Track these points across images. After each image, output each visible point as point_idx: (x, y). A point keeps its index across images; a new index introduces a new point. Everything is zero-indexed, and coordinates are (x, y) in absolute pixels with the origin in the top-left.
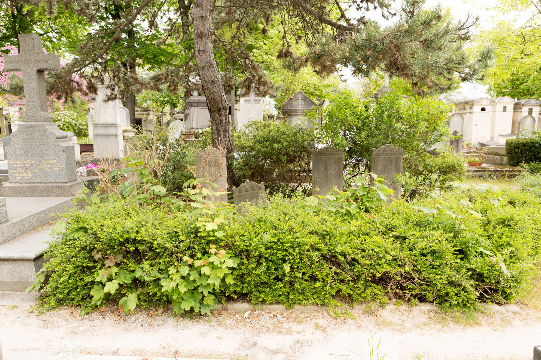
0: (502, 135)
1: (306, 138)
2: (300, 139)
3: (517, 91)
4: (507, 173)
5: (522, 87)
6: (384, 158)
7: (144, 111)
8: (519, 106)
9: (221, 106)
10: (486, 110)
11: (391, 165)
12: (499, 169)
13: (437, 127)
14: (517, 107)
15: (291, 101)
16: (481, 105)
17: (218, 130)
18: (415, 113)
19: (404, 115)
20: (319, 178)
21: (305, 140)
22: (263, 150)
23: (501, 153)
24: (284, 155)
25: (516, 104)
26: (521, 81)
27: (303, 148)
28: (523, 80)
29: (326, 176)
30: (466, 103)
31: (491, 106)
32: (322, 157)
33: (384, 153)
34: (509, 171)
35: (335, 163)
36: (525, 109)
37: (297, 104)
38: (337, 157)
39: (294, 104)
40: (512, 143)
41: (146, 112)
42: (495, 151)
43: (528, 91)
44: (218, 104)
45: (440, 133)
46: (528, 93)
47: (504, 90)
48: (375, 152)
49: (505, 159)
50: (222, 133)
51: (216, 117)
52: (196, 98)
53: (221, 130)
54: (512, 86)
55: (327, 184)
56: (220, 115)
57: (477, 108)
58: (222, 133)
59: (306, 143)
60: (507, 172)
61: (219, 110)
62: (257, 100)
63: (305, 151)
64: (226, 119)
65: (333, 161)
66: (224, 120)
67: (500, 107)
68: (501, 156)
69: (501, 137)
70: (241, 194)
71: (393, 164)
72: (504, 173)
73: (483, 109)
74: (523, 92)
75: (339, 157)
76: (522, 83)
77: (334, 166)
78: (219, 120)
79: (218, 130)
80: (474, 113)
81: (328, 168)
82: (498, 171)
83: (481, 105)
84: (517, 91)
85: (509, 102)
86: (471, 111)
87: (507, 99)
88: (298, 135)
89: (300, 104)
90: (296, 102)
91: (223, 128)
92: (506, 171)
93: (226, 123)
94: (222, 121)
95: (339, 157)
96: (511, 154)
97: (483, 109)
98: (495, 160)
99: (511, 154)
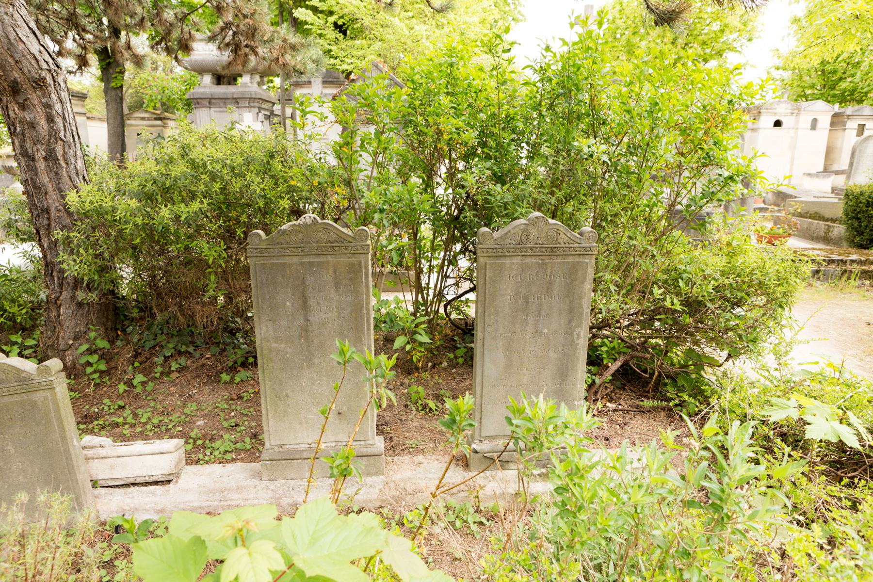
0: (809, 174)
3: (832, 92)
4: (856, 268)
5: (843, 85)
6: (524, 268)
7: (156, 119)
8: (840, 119)
9: (16, 75)
10: (784, 125)
11: (549, 290)
12: (835, 257)
13: (716, 153)
14: (837, 121)
16: (775, 114)
18: (645, 104)
19: (613, 115)
20: (277, 339)
23: (827, 214)
25: (836, 115)
26: (839, 74)
28: (844, 73)
29: (306, 331)
31: (793, 118)
32: (287, 260)
33: (521, 247)
34: (860, 263)
35: (337, 285)
36: (852, 125)
38: (344, 260)
40: (862, 194)
41: (159, 122)
42: (813, 210)
43: (853, 92)
45: (726, 174)
46: (853, 97)
47: (808, 92)
48: (489, 243)
49: (839, 230)
50: (41, 165)
52: (207, 90)
54: (823, 82)
55: (309, 360)
56: (23, 107)
57: (767, 121)
58: (41, 165)
60: (855, 265)
64: (50, 119)
65: (328, 277)
67: (805, 120)
68: (827, 220)
69: (808, 178)
71: (556, 290)
72: (848, 267)
73: (778, 124)
74: (843, 94)
75: (354, 260)
76: (841, 79)
77: (334, 296)
80: (760, 131)
81: (312, 302)
82: (833, 261)
83: (775, 114)
84: (832, 92)
85: (823, 111)
86: (755, 126)
87: (821, 104)
92: (853, 261)
93: (53, 134)
94: (32, 125)
95: (354, 260)
96: (858, 219)
97: (778, 124)
98: (813, 228)
99: (858, 219)
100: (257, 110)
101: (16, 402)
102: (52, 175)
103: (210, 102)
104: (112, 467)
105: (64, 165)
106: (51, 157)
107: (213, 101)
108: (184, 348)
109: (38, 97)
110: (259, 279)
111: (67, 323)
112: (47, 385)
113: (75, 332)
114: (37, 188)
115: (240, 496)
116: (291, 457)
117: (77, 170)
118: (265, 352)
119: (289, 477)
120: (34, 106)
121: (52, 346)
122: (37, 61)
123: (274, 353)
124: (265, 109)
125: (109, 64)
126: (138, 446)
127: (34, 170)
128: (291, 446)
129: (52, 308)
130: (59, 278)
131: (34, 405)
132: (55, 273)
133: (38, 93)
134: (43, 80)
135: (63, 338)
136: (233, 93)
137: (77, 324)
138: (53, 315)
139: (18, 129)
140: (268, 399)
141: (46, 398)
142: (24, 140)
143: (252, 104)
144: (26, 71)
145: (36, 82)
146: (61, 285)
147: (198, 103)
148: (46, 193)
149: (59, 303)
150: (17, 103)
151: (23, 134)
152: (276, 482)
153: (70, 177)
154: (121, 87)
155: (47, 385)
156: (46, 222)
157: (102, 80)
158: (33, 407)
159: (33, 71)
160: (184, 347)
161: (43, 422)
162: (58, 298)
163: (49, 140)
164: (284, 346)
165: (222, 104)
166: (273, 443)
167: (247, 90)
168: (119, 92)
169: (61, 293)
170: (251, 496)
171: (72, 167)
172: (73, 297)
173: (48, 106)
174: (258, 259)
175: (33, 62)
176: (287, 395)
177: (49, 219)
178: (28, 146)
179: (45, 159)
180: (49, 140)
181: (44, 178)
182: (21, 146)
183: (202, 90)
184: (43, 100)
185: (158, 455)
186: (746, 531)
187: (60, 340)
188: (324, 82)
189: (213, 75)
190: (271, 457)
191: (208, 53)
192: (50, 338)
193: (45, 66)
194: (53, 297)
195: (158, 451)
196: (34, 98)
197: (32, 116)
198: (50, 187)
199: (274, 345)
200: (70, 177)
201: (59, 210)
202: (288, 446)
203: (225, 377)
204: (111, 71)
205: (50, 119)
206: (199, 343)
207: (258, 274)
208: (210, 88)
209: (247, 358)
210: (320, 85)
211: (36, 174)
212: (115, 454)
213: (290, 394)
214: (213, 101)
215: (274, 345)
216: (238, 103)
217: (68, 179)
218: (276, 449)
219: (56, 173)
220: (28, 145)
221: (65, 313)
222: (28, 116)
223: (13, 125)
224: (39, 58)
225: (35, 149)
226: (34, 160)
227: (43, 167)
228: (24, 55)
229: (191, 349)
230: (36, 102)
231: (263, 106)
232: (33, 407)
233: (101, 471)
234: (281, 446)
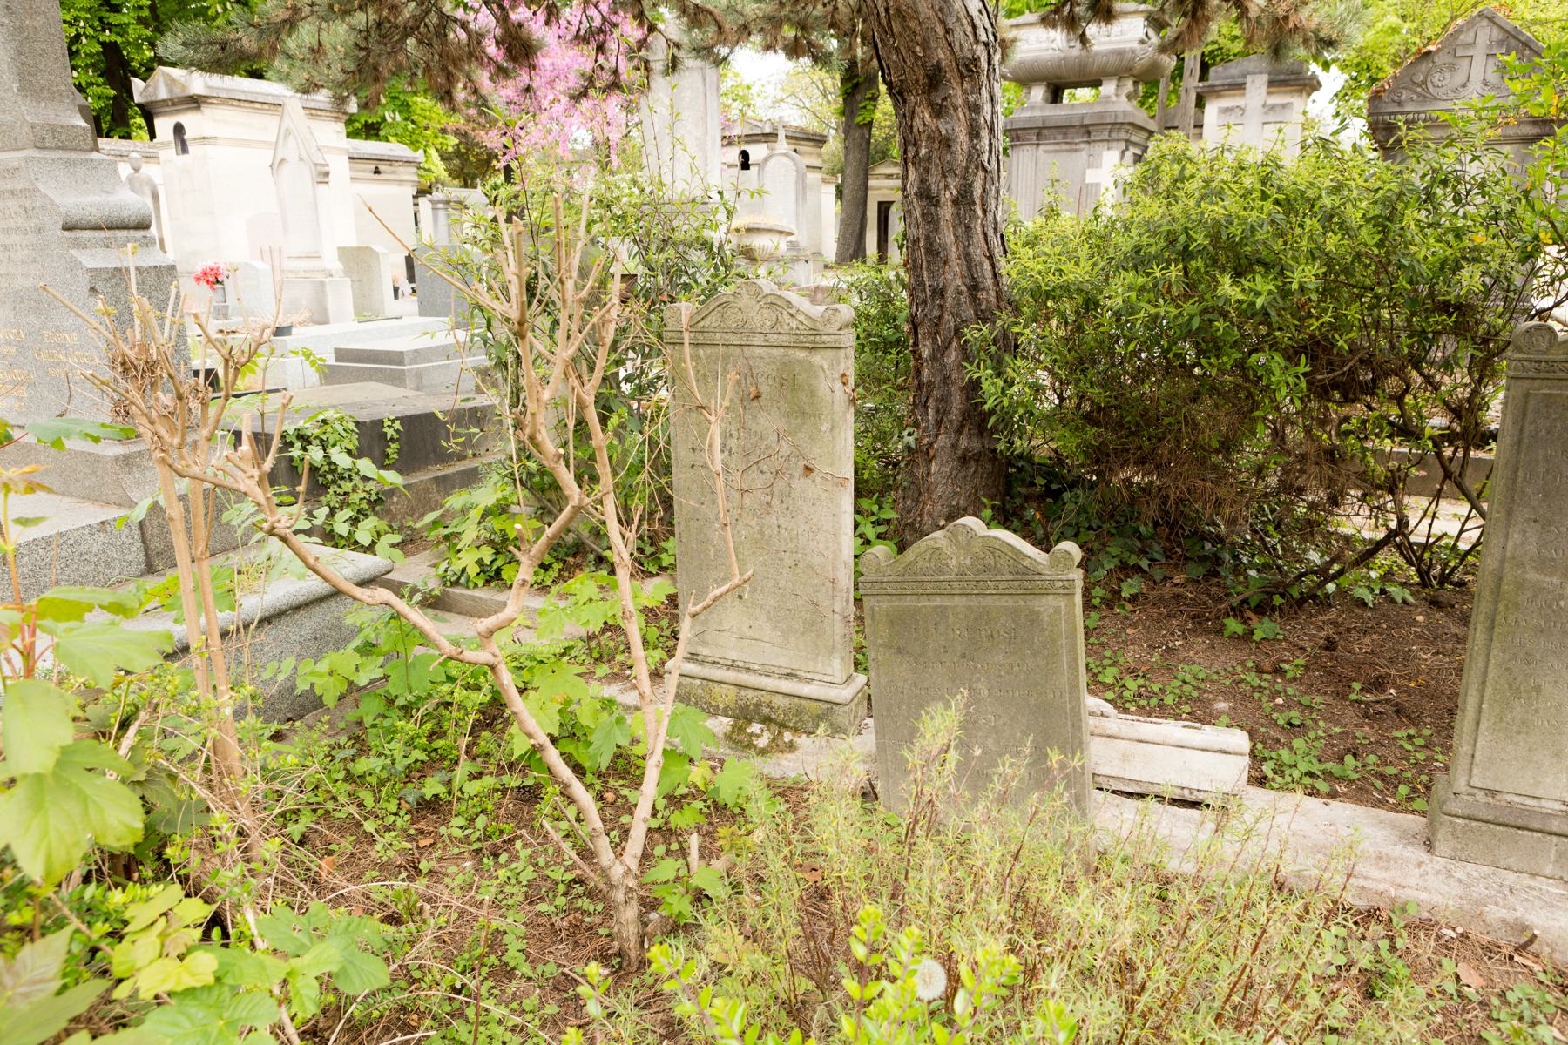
1: (1481, 238)
2: (1427, 250)
9: (941, 55)
15: (1424, 67)
17: (927, 197)
20: (1542, 565)
21: (1474, 256)
22: (1145, 310)
24: (1292, 356)
27: (1445, 307)
30: (430, 606)
37: (1460, 77)
39: (1442, 81)
44: (925, 44)
50: (947, 212)
51: (917, 123)
52: (1037, 114)
53: (946, 197)
56: (938, 112)
58: (947, 212)
59: (1470, 279)
61: (935, 79)
62: (1273, 108)
63: (1460, 331)
64: (974, 133)
66: (963, 138)
70: (909, 602)
78: (930, 139)
79: (927, 197)
88: (1413, 216)
89: (1476, 77)
90: (1453, 68)
91: (953, 182)
93: (973, 155)
94: (947, 143)
100: (1122, 145)
101: (1006, 608)
102: (961, 230)
103: (1038, 136)
104: (1125, 758)
105: (980, 213)
106: (963, 199)
107: (1045, 132)
108: (1133, 560)
109: (964, 92)
110: (1529, 428)
111: (940, 490)
112: (1064, 587)
113: (950, 506)
114: (933, 252)
115: (1384, 875)
116: (1520, 822)
117: (996, 223)
118: (1505, 587)
119: (1502, 863)
120: (955, 108)
121: (912, 524)
122: (974, 27)
123: (1529, 594)
124: (1135, 144)
125: (856, 86)
126: (1171, 729)
127: (931, 220)
128: (1517, 799)
129: (919, 460)
130: (938, 411)
131: (1034, 619)
132: (931, 403)
133: (966, 86)
134: (976, 60)
135: (930, 514)
136: (1083, 116)
137: (955, 493)
138: (919, 472)
139: (923, 151)
140: (1489, 689)
141: (1057, 610)
142: (927, 170)
143: (1114, 135)
144: (957, 47)
145: (966, 66)
146: (939, 423)
147: (1018, 139)
148: (945, 263)
149: (931, 453)
150: (931, 104)
151: (929, 159)
152: (1470, 867)
153: (985, 234)
154: (871, 123)
155: (1064, 587)
156: (936, 313)
157: (843, 113)
158: (1032, 622)
159: (966, 46)
160: (1134, 557)
161: (1045, 652)
162: (931, 445)
163: (967, 168)
164: (1556, 581)
165: (1060, 138)
166: (1476, 782)
167: (1111, 108)
168: (866, 132)
169: (937, 436)
170: (1412, 882)
171: (990, 216)
172: (954, 446)
173: (975, 108)
174: (1537, 383)
175: (969, 29)
176: (1538, 689)
177: (941, 306)
178: (932, 179)
179: (955, 202)
180: (967, 168)
181: (947, 237)
182: (923, 181)
183: (1028, 114)
184: (971, 98)
185: (1210, 755)
186: (950, 1023)
187: (926, 517)
188: (1271, 83)
189: (1048, 85)
190: (1467, 812)
191: (1045, 45)
192: (909, 512)
193: (983, 38)
194: (925, 441)
195: (1217, 747)
196: (956, 92)
197: (949, 126)
198: (953, 252)
199: (1532, 576)
200: (985, 234)
201: (960, 293)
202: (1509, 798)
203: (1233, 625)
204: (858, 97)
205: (974, 133)
206: (1156, 556)
207: (1530, 416)
208: (1042, 109)
209: (1271, 594)
210: (1264, 89)
211: (937, 229)
212: (1135, 735)
213: (1547, 688)
214: (1045, 132)
215: (1532, 576)
216: (1089, 133)
217: (981, 237)
218: (1480, 796)
219: (968, 228)
220: (934, 177)
221: (940, 473)
222: (944, 127)
223: (915, 144)
224: (978, 23)
225: (942, 185)
226: (937, 204)
227: (949, 216)
228: (959, 19)
229: (1144, 563)
230: (960, 102)
231: (1133, 138)
232: (1032, 622)
233: (1103, 757)
234: (1493, 793)
